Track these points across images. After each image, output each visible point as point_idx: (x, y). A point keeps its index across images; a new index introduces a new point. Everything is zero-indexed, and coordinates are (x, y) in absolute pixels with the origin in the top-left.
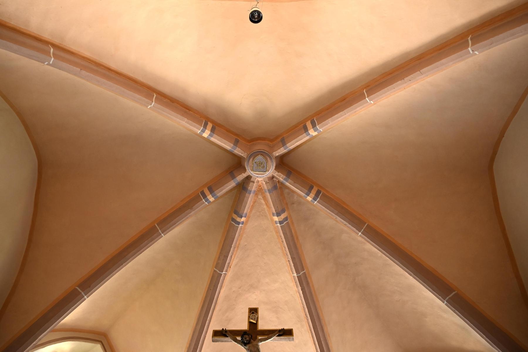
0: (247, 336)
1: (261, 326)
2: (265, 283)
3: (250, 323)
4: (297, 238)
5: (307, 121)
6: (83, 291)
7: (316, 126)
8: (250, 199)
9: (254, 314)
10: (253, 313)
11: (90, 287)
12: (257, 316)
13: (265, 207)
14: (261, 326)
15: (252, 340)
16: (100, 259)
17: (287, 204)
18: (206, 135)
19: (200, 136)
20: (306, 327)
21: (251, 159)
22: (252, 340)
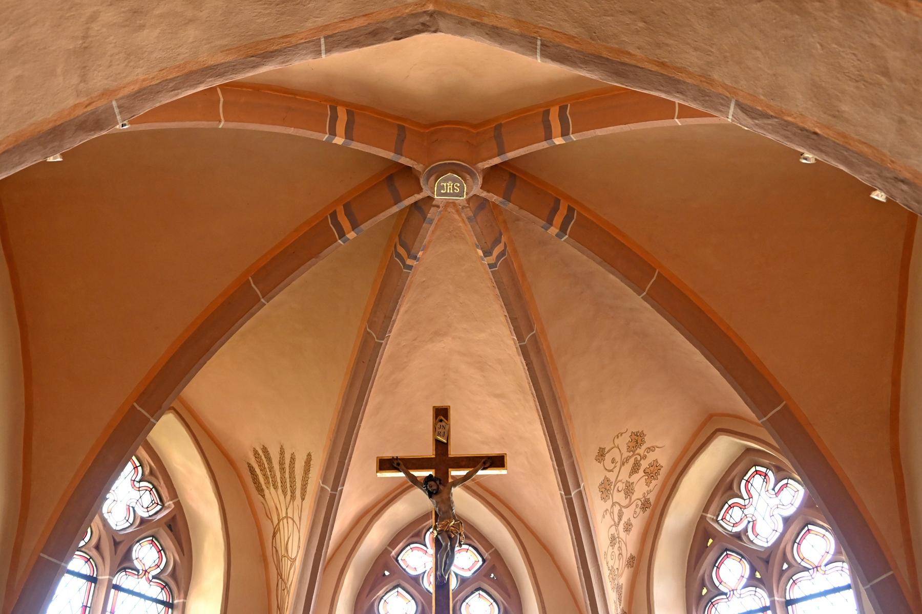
0: (432, 483)
1: (453, 452)
2: (461, 359)
3: (437, 442)
4: (524, 275)
5: (553, 106)
6: (152, 416)
7: (568, 134)
8: (429, 232)
9: (443, 424)
10: (441, 421)
11: (160, 408)
12: (447, 427)
13: (461, 224)
14: (453, 452)
15: (441, 487)
16: (199, 438)
17: (505, 222)
18: (339, 141)
19: (328, 143)
20: (532, 403)
21: (433, 178)
22: (441, 487)
